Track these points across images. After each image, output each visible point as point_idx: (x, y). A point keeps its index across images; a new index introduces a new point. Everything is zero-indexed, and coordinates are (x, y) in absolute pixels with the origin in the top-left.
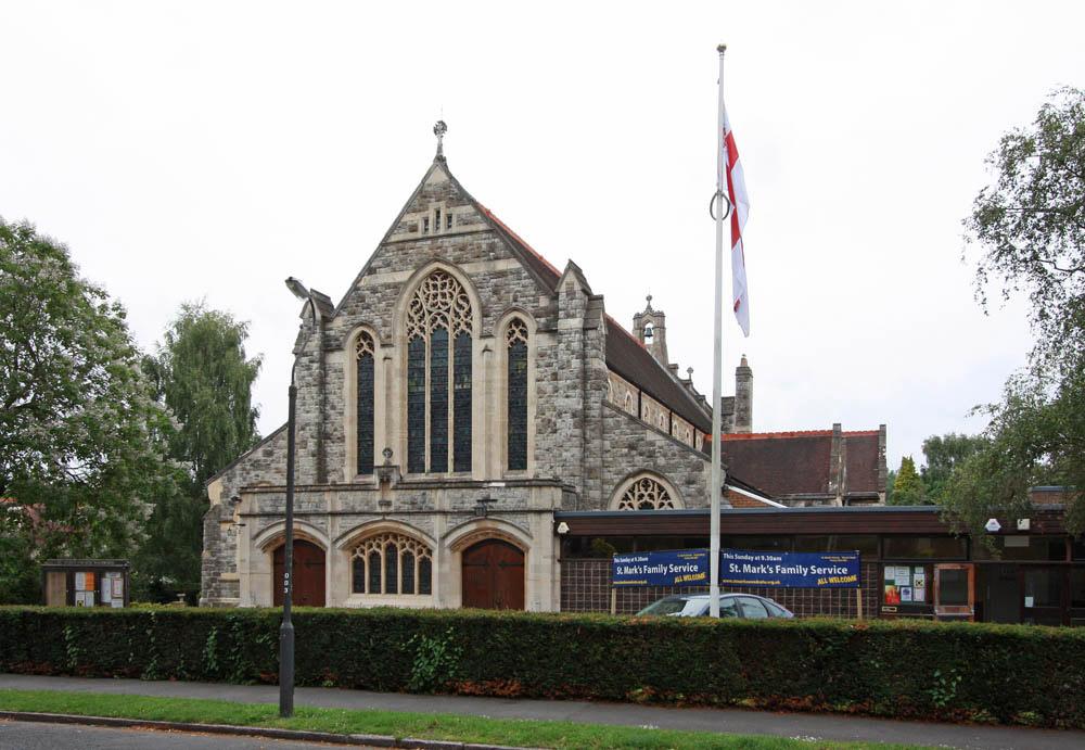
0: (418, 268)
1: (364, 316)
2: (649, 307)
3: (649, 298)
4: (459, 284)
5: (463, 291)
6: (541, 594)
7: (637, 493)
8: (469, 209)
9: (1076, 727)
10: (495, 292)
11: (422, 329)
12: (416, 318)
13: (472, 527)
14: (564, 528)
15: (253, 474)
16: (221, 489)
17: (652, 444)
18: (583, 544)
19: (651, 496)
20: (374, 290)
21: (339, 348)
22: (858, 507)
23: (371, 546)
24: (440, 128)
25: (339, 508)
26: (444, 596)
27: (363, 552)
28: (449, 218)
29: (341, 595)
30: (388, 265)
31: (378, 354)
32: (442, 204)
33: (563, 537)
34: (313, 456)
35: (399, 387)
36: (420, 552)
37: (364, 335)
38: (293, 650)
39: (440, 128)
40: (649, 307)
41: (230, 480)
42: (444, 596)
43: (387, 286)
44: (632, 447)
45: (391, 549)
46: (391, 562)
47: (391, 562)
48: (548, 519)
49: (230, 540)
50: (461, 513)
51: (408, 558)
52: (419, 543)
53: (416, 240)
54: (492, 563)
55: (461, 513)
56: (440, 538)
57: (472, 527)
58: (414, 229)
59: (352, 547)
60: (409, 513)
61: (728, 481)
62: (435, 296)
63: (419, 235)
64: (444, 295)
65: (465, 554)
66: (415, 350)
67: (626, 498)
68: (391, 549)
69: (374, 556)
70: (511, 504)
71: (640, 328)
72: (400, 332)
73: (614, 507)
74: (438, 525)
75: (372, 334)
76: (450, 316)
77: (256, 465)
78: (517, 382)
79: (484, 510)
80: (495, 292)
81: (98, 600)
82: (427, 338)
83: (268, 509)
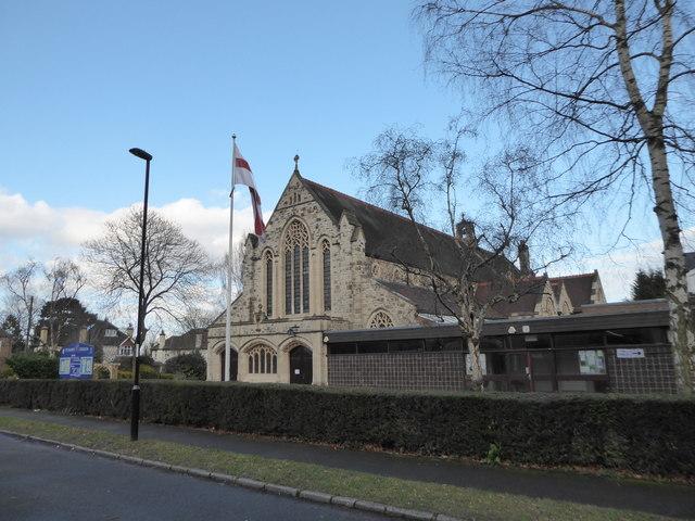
6: (320, 375)
13: (290, 340)
14: (326, 339)
18: (336, 347)
22: (577, 315)
24: (297, 158)
25: (242, 333)
26: (281, 377)
31: (274, 260)
33: (328, 344)
34: (106, 320)
37: (269, 252)
38: (422, 392)
39: (297, 158)
42: (281, 377)
45: (263, 351)
48: (319, 335)
51: (269, 355)
56: (279, 344)
59: (248, 351)
61: (418, 311)
65: (291, 353)
68: (263, 351)
69: (256, 355)
70: (304, 329)
71: (460, 232)
72: (281, 249)
73: (368, 327)
74: (277, 340)
76: (301, 240)
78: (327, 269)
82: (292, 251)
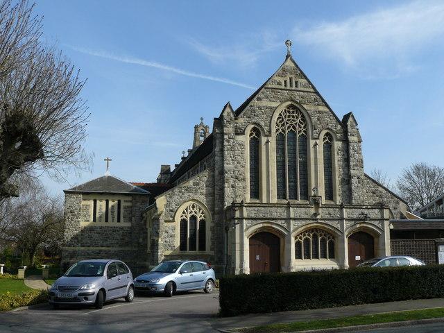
0: (282, 102)
1: (255, 119)
2: (202, 123)
3: (202, 119)
4: (301, 113)
5: (303, 116)
7: (189, 211)
8: (304, 81)
9: (439, 296)
10: (319, 120)
11: (284, 131)
12: (280, 124)
15: (186, 195)
16: (165, 202)
17: (381, 192)
19: (196, 213)
20: (260, 108)
21: (243, 133)
23: (305, 235)
27: (301, 238)
28: (296, 83)
29: (389, 258)
30: (267, 98)
31: (264, 140)
32: (293, 76)
35: (273, 156)
36: (329, 238)
40: (202, 123)
41: (171, 197)
43: (267, 107)
44: (374, 193)
45: (315, 237)
46: (315, 243)
47: (315, 243)
49: (170, 232)
50: (352, 220)
52: (301, 234)
53: (281, 89)
54: (365, 240)
55: (352, 220)
57: (315, 224)
58: (279, 84)
60: (329, 219)
62: (289, 116)
63: (283, 87)
64: (289, 116)
66: (281, 139)
67: (184, 213)
69: (307, 241)
75: (331, 133)
77: (188, 189)
79: (365, 218)
80: (319, 120)
81: (241, 271)
83: (253, 216)
